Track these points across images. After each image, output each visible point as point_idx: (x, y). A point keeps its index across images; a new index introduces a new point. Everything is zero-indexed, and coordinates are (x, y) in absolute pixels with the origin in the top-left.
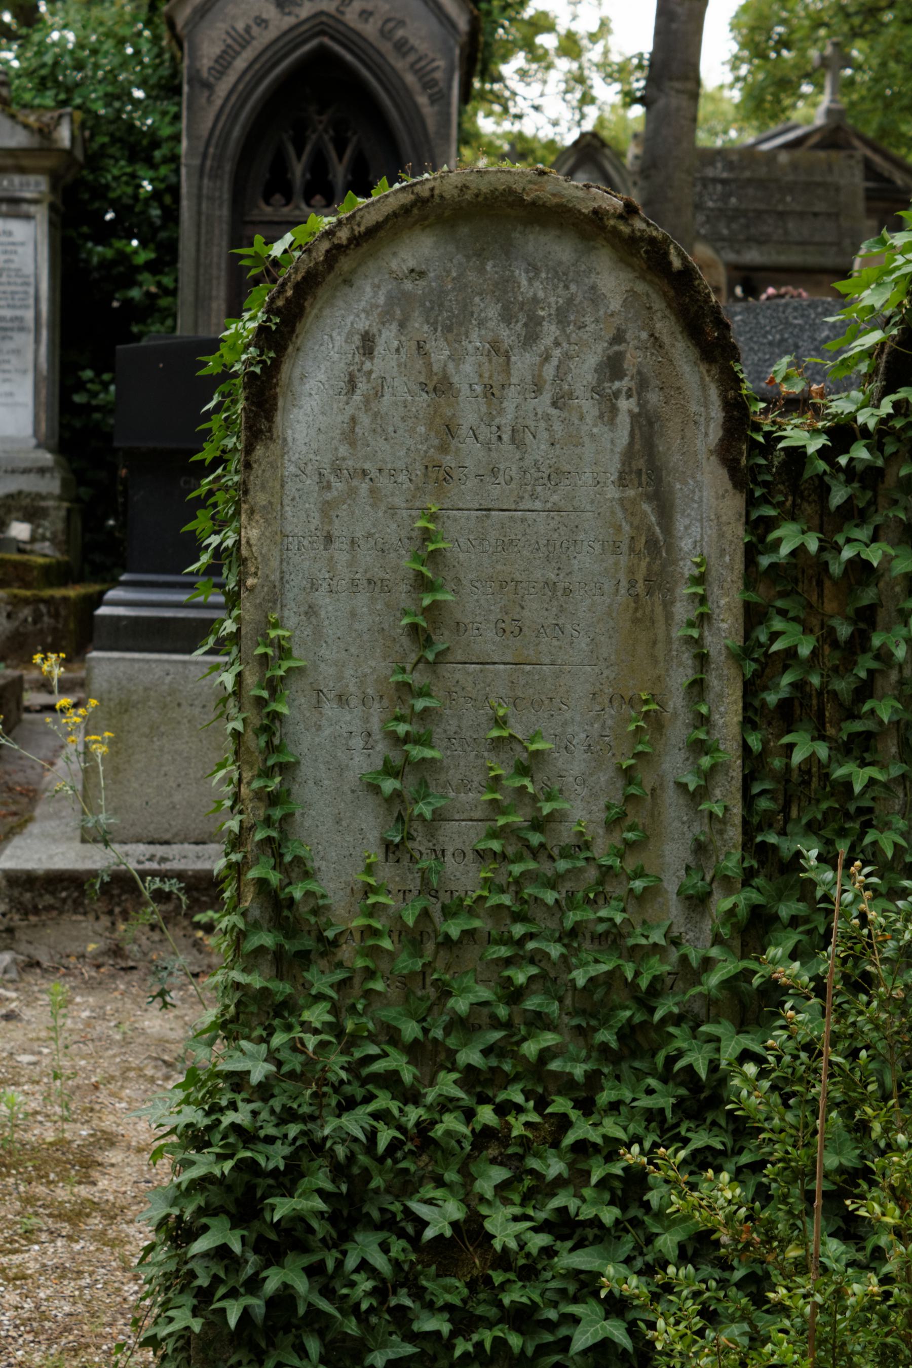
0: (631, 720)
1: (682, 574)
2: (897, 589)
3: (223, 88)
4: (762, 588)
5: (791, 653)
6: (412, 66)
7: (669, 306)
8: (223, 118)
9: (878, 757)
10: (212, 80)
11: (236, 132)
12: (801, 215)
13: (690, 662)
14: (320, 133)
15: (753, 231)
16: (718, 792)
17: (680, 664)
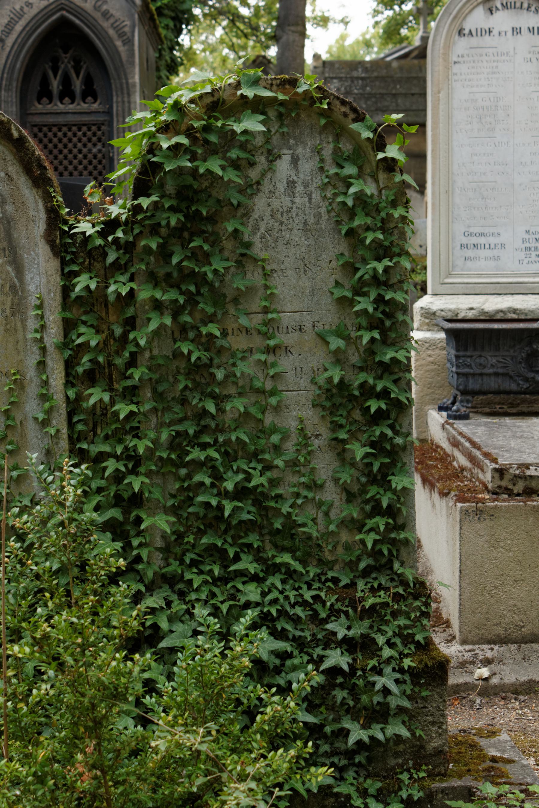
0: (7, 385)
1: (31, 304)
2: (147, 307)
3: (10, 41)
4: (74, 310)
5: (86, 344)
6: (112, 25)
7: (15, 158)
8: (11, 57)
9: (140, 399)
10: (3, 37)
11: (18, 65)
12: (405, 95)
13: (37, 352)
14: (66, 63)
15: (379, 105)
16: (54, 422)
17: (32, 353)
